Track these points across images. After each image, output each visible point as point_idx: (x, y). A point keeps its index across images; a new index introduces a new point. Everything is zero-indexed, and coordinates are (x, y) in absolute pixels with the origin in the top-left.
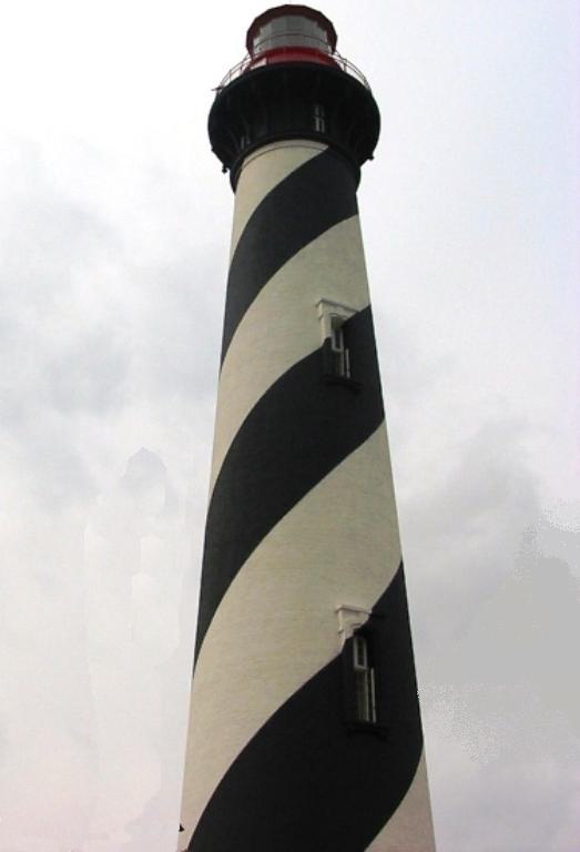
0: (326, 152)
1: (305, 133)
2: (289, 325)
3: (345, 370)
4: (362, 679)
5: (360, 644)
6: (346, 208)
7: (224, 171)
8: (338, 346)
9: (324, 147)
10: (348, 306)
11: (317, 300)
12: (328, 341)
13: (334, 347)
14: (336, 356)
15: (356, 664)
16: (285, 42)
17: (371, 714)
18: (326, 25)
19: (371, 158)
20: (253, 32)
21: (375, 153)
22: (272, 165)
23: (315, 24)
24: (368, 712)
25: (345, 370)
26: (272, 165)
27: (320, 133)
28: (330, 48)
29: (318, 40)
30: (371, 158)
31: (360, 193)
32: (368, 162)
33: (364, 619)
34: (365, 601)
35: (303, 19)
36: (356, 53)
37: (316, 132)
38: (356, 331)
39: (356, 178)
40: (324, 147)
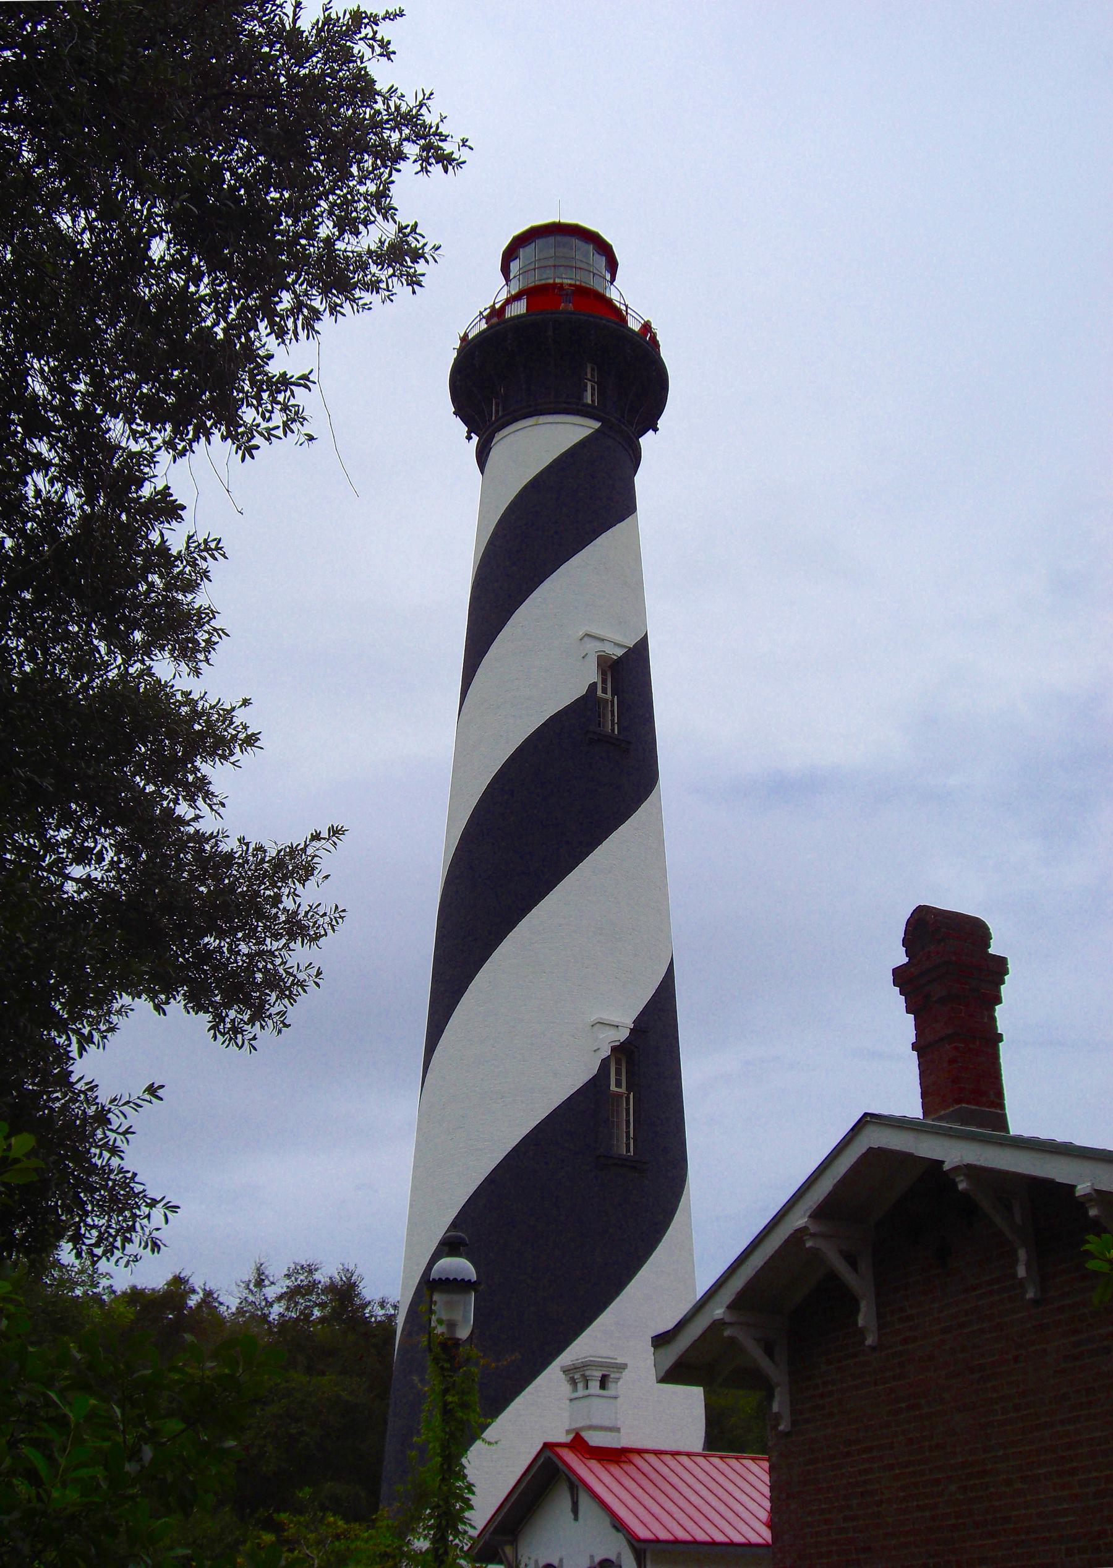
0: (597, 431)
1: (573, 407)
2: (547, 665)
3: (611, 725)
4: (605, 708)
5: (618, 1063)
6: (622, 505)
7: (469, 438)
8: (604, 691)
9: (597, 425)
10: (661, 1351)
11: (581, 633)
12: (593, 687)
13: (599, 693)
14: (599, 702)
15: (613, 1088)
16: (549, 277)
17: (613, 730)
18: (604, 249)
19: (656, 430)
20: (510, 255)
21: (661, 423)
22: (541, 442)
23: (591, 248)
24: (624, 1145)
25: (613, 725)
26: (541, 442)
27: (592, 406)
28: (608, 277)
29: (584, 270)
30: (656, 430)
31: (905, 1027)
32: (651, 432)
33: (623, 1035)
34: (623, 1015)
35: (576, 242)
36: (636, 294)
37: (588, 405)
38: (627, 675)
39: (993, 1019)
40: (597, 425)
